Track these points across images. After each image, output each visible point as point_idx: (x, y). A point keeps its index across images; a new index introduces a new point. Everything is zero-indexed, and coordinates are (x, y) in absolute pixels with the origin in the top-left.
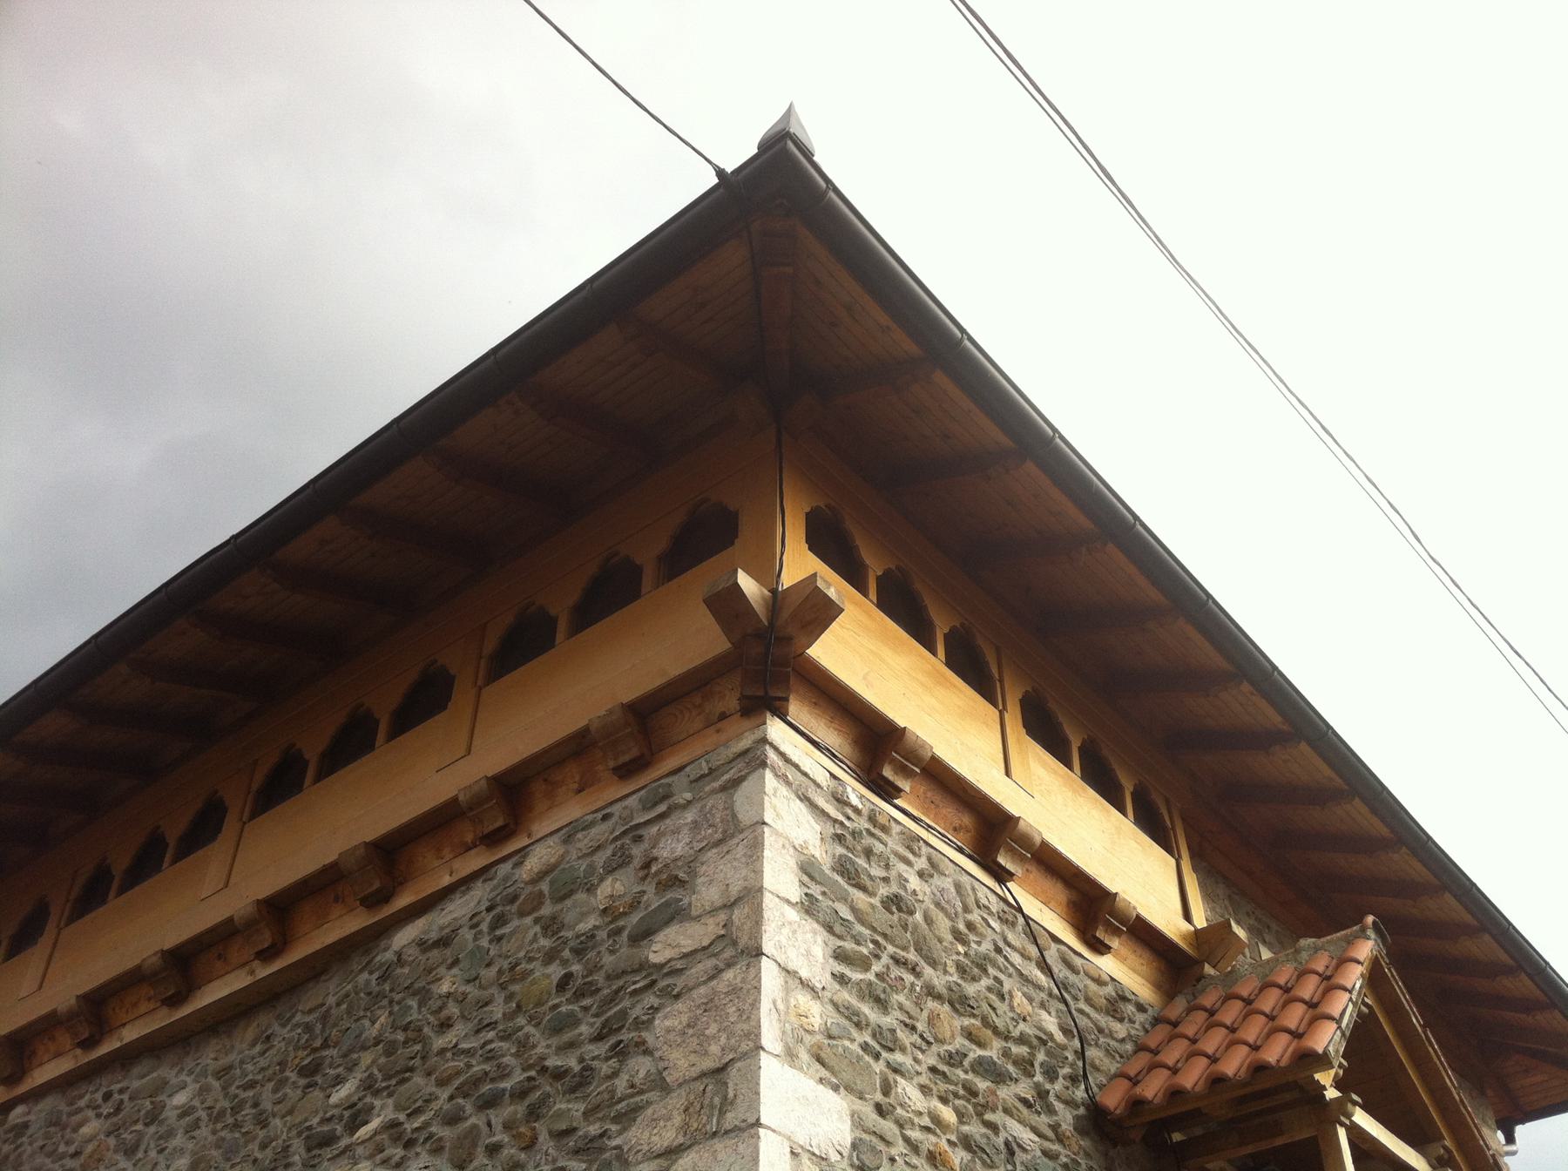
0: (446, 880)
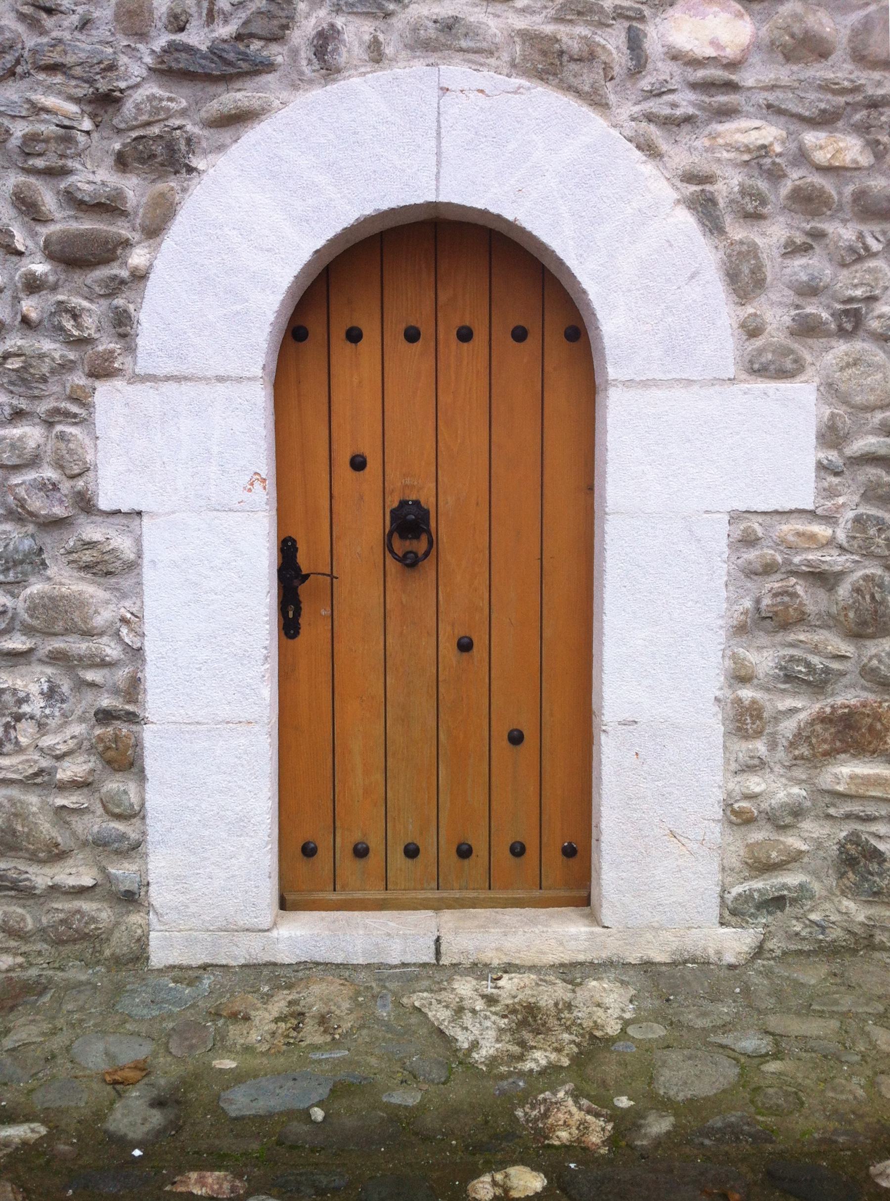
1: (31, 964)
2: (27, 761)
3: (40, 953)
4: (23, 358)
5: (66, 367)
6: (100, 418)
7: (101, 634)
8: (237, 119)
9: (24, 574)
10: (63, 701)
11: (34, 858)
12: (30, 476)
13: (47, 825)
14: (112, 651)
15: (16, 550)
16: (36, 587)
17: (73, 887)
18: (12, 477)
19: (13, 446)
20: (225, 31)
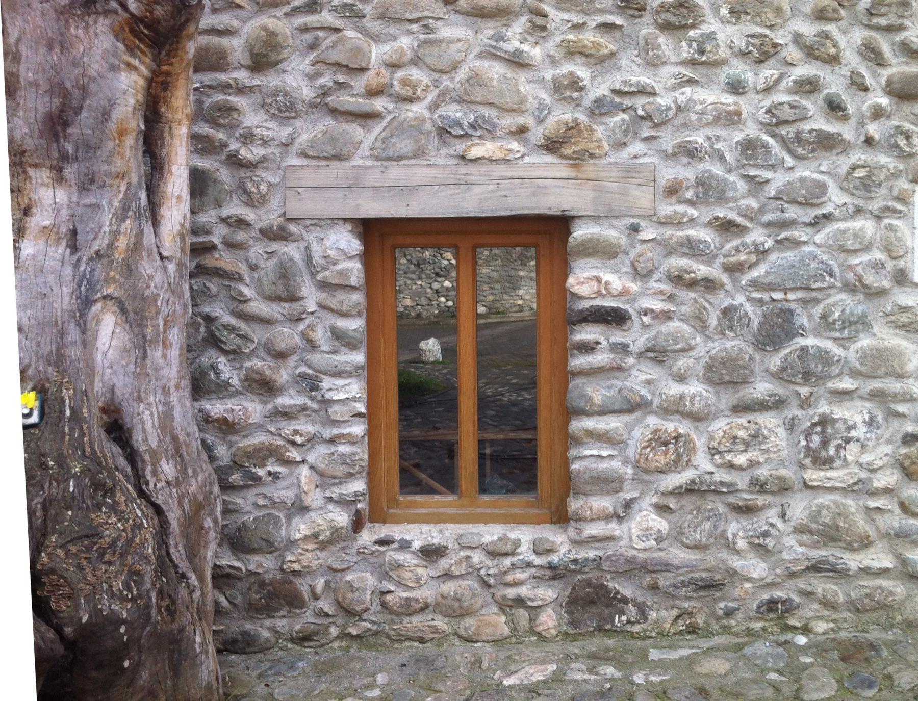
1: (840, 628)
2: (850, 473)
3: (845, 620)
4: (868, 169)
5: (896, 175)
7: (909, 377)
9: (857, 332)
10: (878, 428)
11: (850, 548)
12: (865, 258)
13: (862, 522)
15: (852, 314)
16: (865, 342)
17: (880, 569)
18: (850, 259)
19: (856, 236)
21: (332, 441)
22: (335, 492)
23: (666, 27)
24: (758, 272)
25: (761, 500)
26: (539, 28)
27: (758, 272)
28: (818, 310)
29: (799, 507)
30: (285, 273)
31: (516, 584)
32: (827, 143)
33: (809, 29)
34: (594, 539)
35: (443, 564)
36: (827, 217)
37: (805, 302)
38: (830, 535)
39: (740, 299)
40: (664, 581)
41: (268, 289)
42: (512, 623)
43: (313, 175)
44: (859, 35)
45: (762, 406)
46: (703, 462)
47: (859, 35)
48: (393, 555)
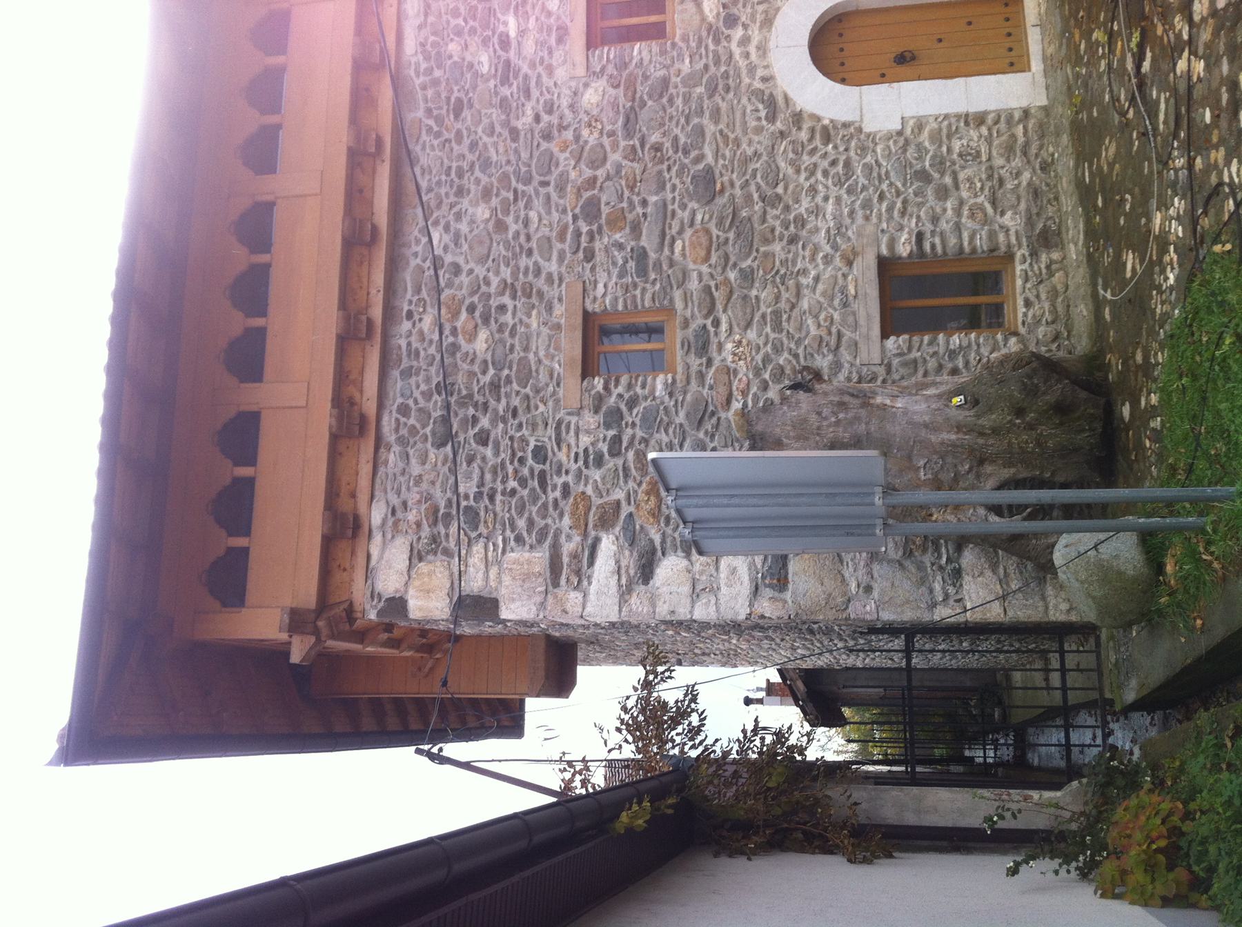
0: (394, 10)
6: (873, 130)
8: (787, 99)
11: (1016, 140)
14: (946, 123)
16: (927, 144)
20: (761, 107)
21: (978, 345)
22: (1001, 344)
23: (803, 226)
24: (899, 185)
25: (996, 176)
26: (804, 272)
27: (899, 185)
28: (914, 162)
29: (998, 162)
30: (905, 364)
31: (1040, 269)
32: (847, 164)
33: (803, 175)
34: (1017, 238)
35: (1032, 298)
36: (876, 161)
37: (911, 167)
38: (1009, 150)
39: (910, 190)
40: (1034, 211)
41: (912, 371)
42: (1058, 270)
43: (863, 356)
44: (805, 157)
45: (955, 179)
46: (980, 199)
47: (805, 157)
48: (1029, 319)
